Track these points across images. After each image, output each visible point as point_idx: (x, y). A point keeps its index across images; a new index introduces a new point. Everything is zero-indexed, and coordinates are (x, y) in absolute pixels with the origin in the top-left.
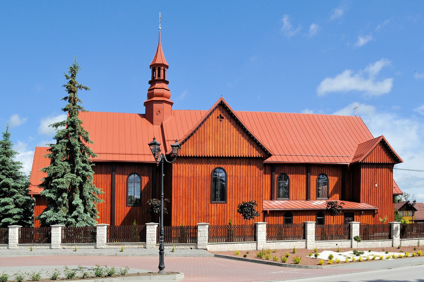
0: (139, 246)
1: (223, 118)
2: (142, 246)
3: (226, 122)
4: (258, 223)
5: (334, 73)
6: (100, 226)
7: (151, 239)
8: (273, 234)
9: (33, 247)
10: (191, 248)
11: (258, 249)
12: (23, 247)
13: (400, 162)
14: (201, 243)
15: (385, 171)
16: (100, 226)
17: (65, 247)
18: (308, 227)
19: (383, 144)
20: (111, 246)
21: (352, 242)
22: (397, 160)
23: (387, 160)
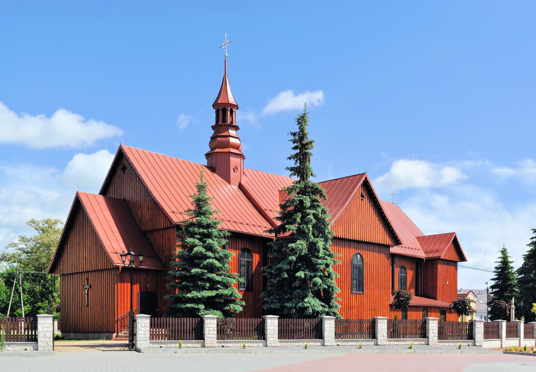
0: (421, 343)
1: (363, 197)
2: (423, 343)
3: (366, 200)
4: (378, 317)
5: (274, 94)
6: (382, 319)
7: (433, 335)
8: (338, 332)
9: (246, 345)
10: (468, 345)
11: (503, 346)
12: (285, 344)
13: (466, 261)
14: (479, 339)
15: (451, 268)
16: (382, 319)
17: (340, 343)
18: (430, 325)
19: (455, 242)
20: (392, 343)
21: (520, 340)
22: (462, 258)
23: (454, 256)
